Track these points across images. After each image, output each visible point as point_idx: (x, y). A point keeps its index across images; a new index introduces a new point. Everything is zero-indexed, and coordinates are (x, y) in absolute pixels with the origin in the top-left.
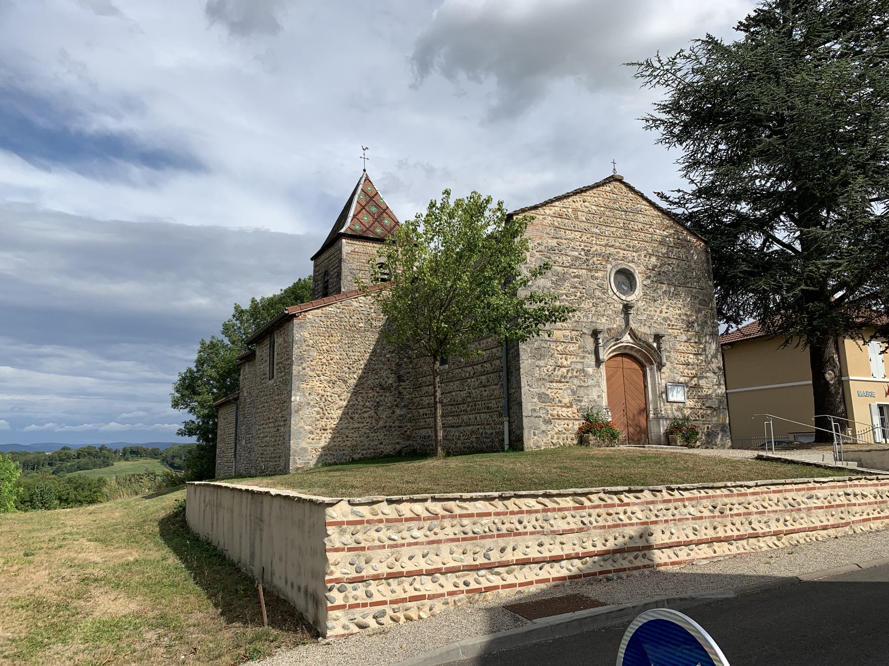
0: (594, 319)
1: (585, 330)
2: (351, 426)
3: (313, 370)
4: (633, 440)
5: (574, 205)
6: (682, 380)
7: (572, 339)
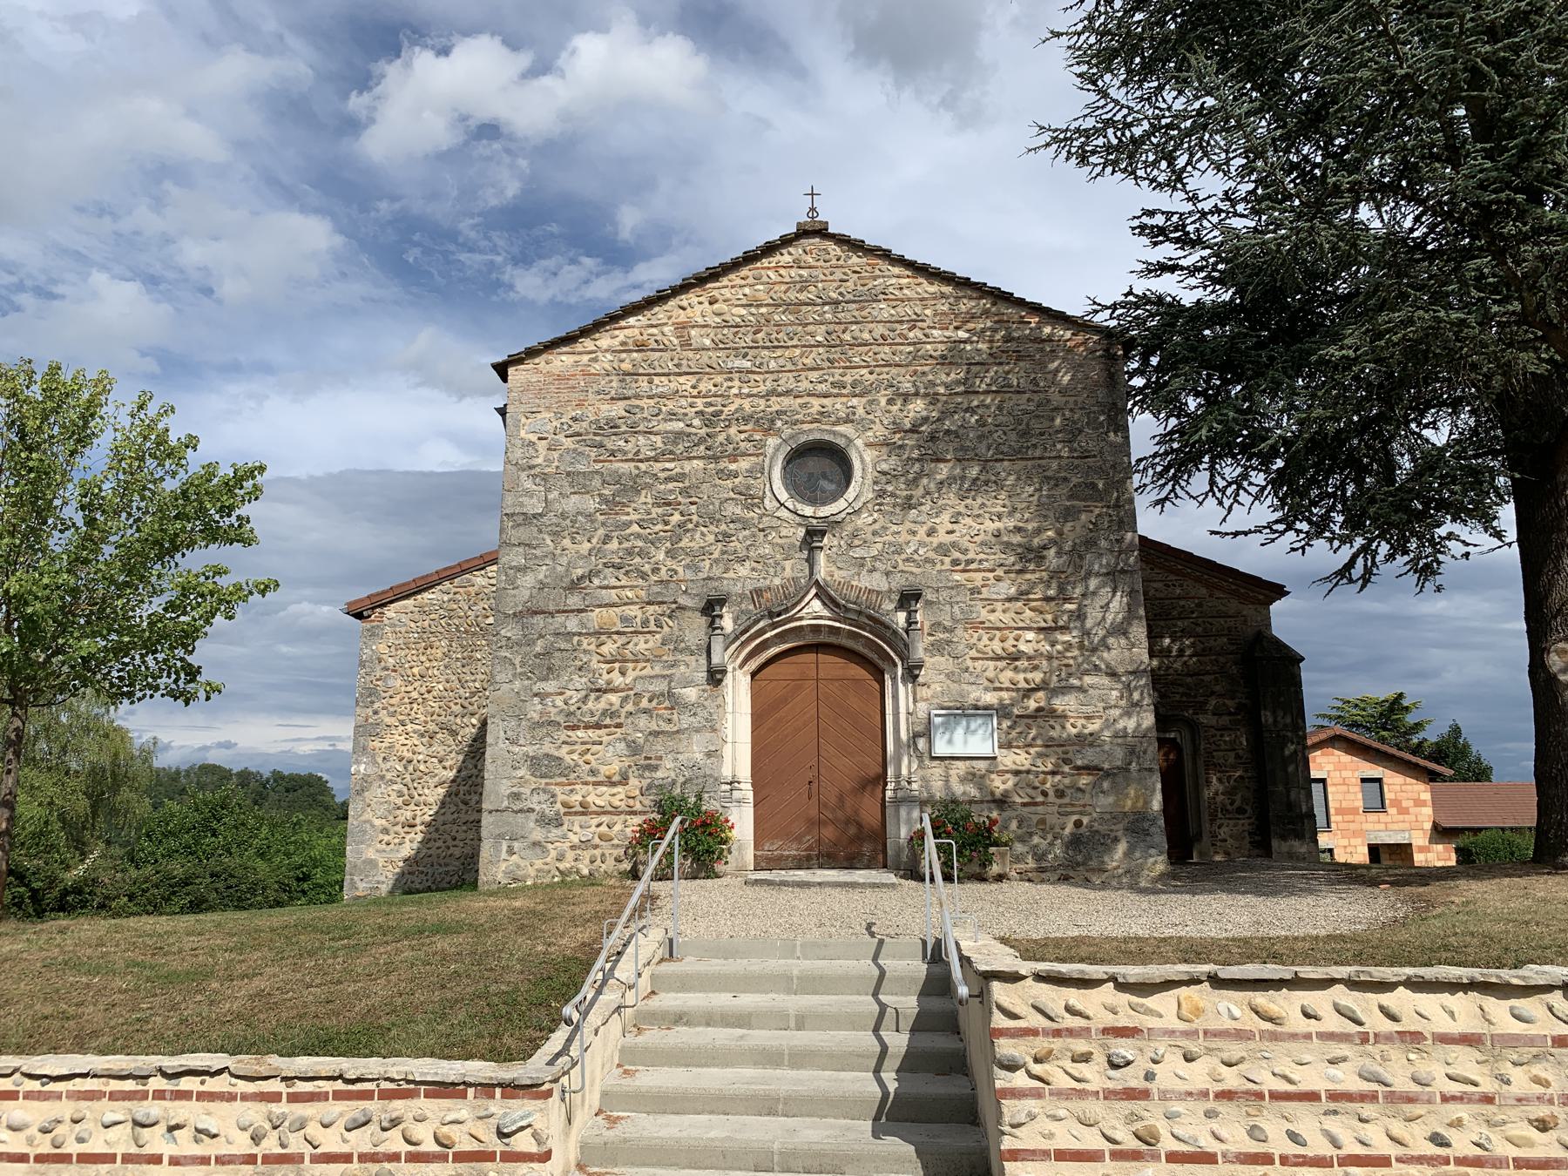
0: (717, 572)
1: (683, 600)
2: (464, 818)
3: (393, 714)
4: (829, 856)
5: (682, 317)
6: (990, 698)
7: (645, 623)
